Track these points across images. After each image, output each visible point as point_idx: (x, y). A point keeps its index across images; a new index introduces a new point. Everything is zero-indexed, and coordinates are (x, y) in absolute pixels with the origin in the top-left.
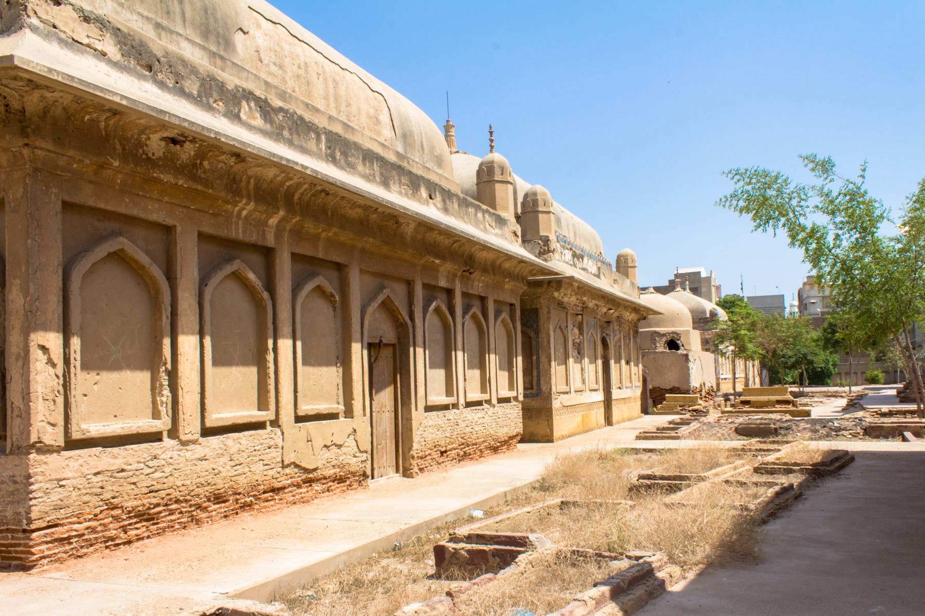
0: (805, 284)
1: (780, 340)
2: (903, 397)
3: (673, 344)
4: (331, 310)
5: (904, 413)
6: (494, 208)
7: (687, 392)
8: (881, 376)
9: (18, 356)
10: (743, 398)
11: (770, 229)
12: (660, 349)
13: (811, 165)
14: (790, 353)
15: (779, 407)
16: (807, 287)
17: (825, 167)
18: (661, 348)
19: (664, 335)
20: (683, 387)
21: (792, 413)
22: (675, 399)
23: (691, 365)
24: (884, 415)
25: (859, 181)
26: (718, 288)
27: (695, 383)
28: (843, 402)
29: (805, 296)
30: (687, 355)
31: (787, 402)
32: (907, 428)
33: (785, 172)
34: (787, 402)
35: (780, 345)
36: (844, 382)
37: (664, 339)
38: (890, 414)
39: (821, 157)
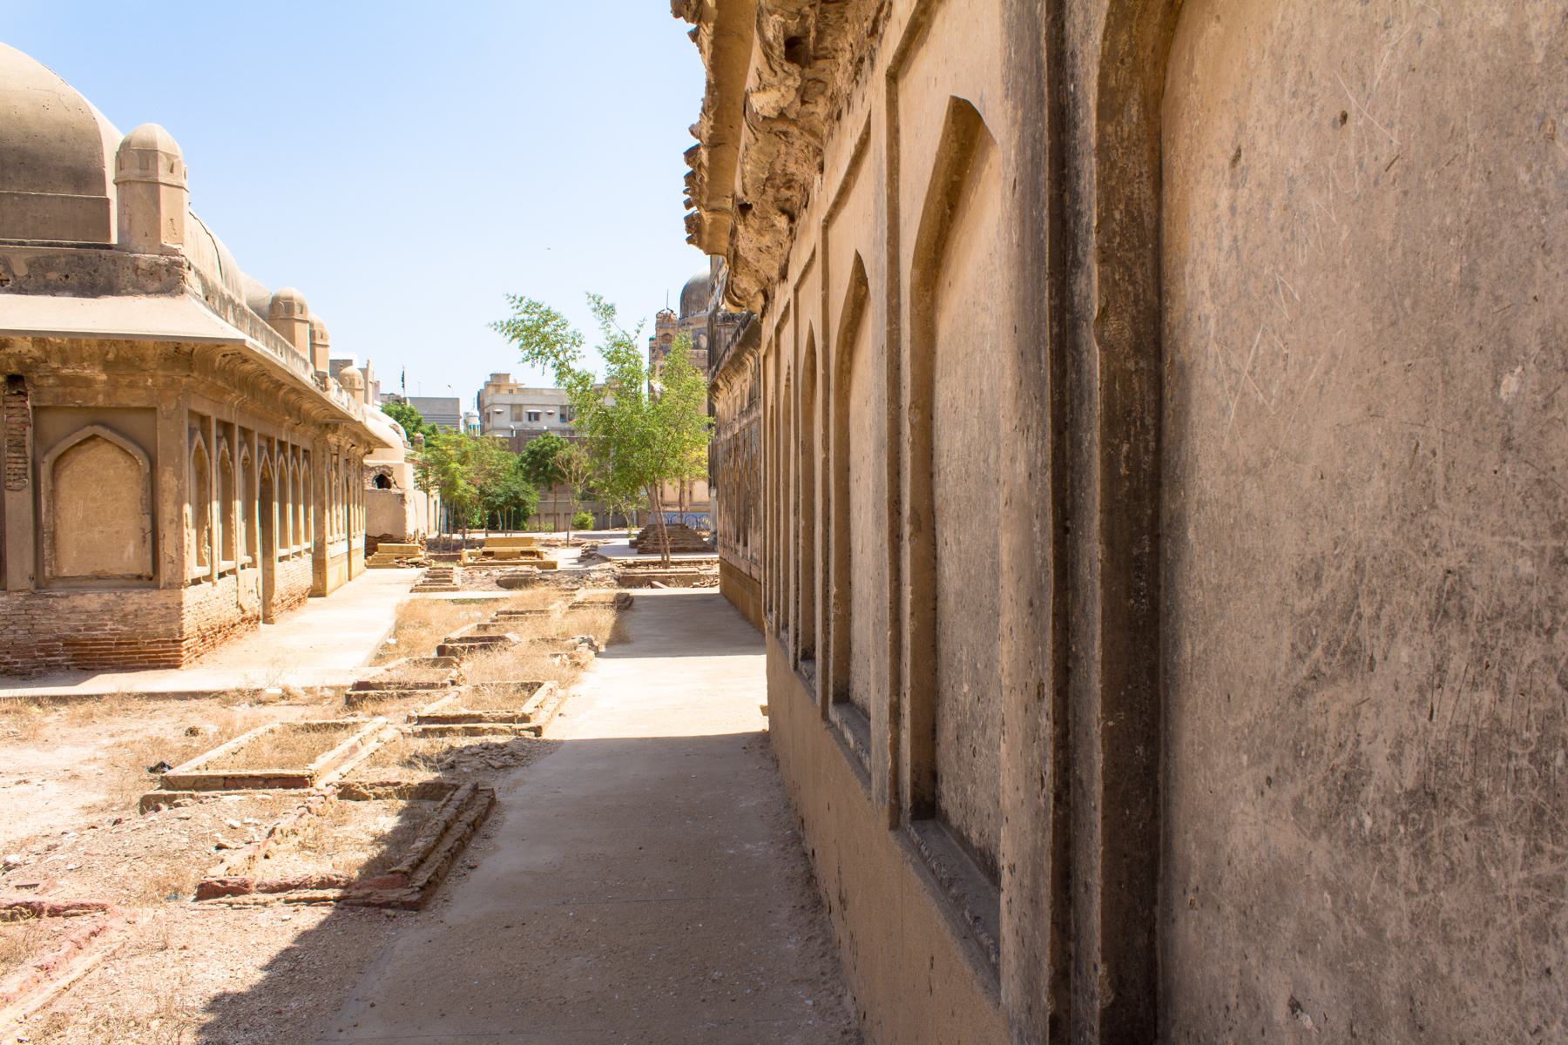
0: (487, 384)
1: (490, 475)
2: (639, 546)
3: (383, 481)
4: (105, 447)
5: (647, 564)
6: (293, 343)
7: (402, 540)
8: (591, 519)
9: (172, 521)
10: (485, 549)
11: (539, 366)
12: (368, 487)
13: (594, 305)
14: (499, 491)
15: (523, 559)
16: (491, 390)
17: (609, 311)
18: (370, 486)
19: (373, 469)
20: (397, 535)
21: (540, 566)
22: (390, 550)
23: (408, 507)
24: (629, 566)
25: (633, 334)
26: (376, 385)
27: (410, 530)
28: (578, 552)
29: (487, 402)
30: (403, 496)
31: (532, 553)
32: (654, 578)
33: (566, 315)
34: (532, 553)
35: (489, 481)
36: (543, 525)
37: (373, 474)
38: (635, 565)
39: (607, 301)
